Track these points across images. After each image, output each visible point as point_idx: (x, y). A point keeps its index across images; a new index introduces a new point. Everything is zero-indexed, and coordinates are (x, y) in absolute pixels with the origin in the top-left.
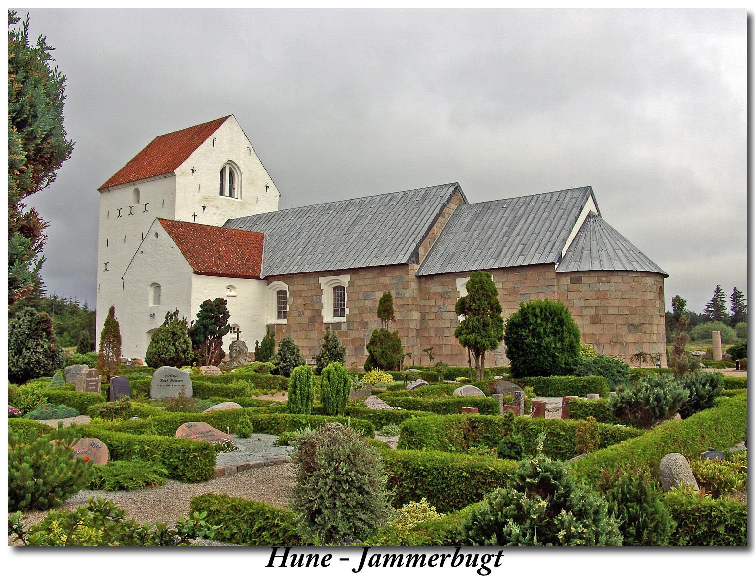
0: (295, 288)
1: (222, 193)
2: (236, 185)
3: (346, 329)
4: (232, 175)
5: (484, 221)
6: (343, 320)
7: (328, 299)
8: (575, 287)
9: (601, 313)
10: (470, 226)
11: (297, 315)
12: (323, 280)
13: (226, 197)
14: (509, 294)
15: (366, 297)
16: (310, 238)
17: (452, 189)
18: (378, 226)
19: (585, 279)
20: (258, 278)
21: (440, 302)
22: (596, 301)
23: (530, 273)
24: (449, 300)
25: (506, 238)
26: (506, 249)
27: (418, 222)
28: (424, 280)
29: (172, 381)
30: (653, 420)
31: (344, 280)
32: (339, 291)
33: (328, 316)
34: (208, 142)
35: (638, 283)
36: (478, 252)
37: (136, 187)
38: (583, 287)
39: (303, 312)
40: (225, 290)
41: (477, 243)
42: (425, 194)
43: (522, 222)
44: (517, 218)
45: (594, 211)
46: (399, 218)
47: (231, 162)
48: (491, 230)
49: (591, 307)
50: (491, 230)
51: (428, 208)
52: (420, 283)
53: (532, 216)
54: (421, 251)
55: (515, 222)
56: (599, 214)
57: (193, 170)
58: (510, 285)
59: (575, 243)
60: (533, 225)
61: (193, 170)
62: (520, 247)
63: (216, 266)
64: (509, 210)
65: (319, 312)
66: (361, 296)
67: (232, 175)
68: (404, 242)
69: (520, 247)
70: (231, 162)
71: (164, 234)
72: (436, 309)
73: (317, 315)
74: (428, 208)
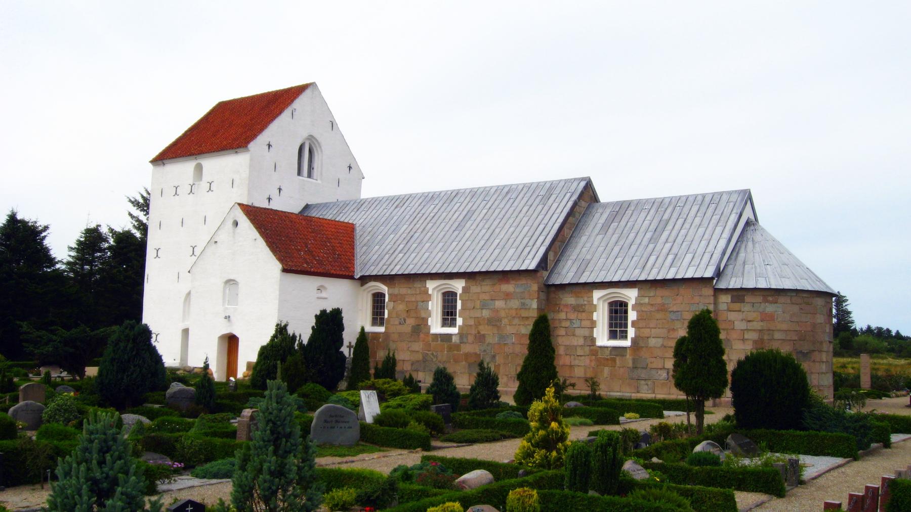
0: (396, 291)
1: (299, 173)
2: (316, 164)
3: (458, 341)
4: (311, 152)
5: (623, 223)
6: (454, 331)
7: (435, 307)
8: (737, 306)
9: (766, 337)
10: (605, 228)
11: (397, 323)
12: (431, 285)
13: (304, 178)
14: (658, 310)
15: (483, 306)
16: (412, 233)
17: (583, 184)
18: (496, 223)
19: (748, 298)
20: (351, 277)
21: (572, 316)
22: (761, 324)
23: (683, 290)
24: (584, 314)
25: (651, 246)
26: (653, 258)
27: (545, 221)
28: (553, 289)
29: (337, 421)
30: (764, 444)
31: (458, 286)
32: (449, 298)
33: (436, 327)
34: (286, 114)
35: (808, 304)
36: (619, 260)
37: (199, 161)
38: (746, 307)
39: (405, 320)
40: (316, 291)
41: (617, 249)
42: (549, 190)
43: (669, 227)
44: (663, 223)
45: (752, 218)
46: (521, 215)
47: (311, 138)
48: (632, 235)
49: (754, 330)
50: (632, 235)
51: (555, 205)
52: (548, 294)
53: (680, 221)
54: (551, 256)
55: (661, 226)
56: (756, 219)
57: (269, 146)
58: (659, 300)
59: (735, 254)
60: (683, 232)
61: (269, 146)
62: (671, 257)
63: (307, 263)
64: (652, 212)
65: (425, 320)
66: (478, 303)
67: (311, 152)
68: (531, 244)
69: (671, 257)
70: (311, 138)
71: (245, 223)
72: (567, 324)
73: (421, 326)
74: (555, 205)
